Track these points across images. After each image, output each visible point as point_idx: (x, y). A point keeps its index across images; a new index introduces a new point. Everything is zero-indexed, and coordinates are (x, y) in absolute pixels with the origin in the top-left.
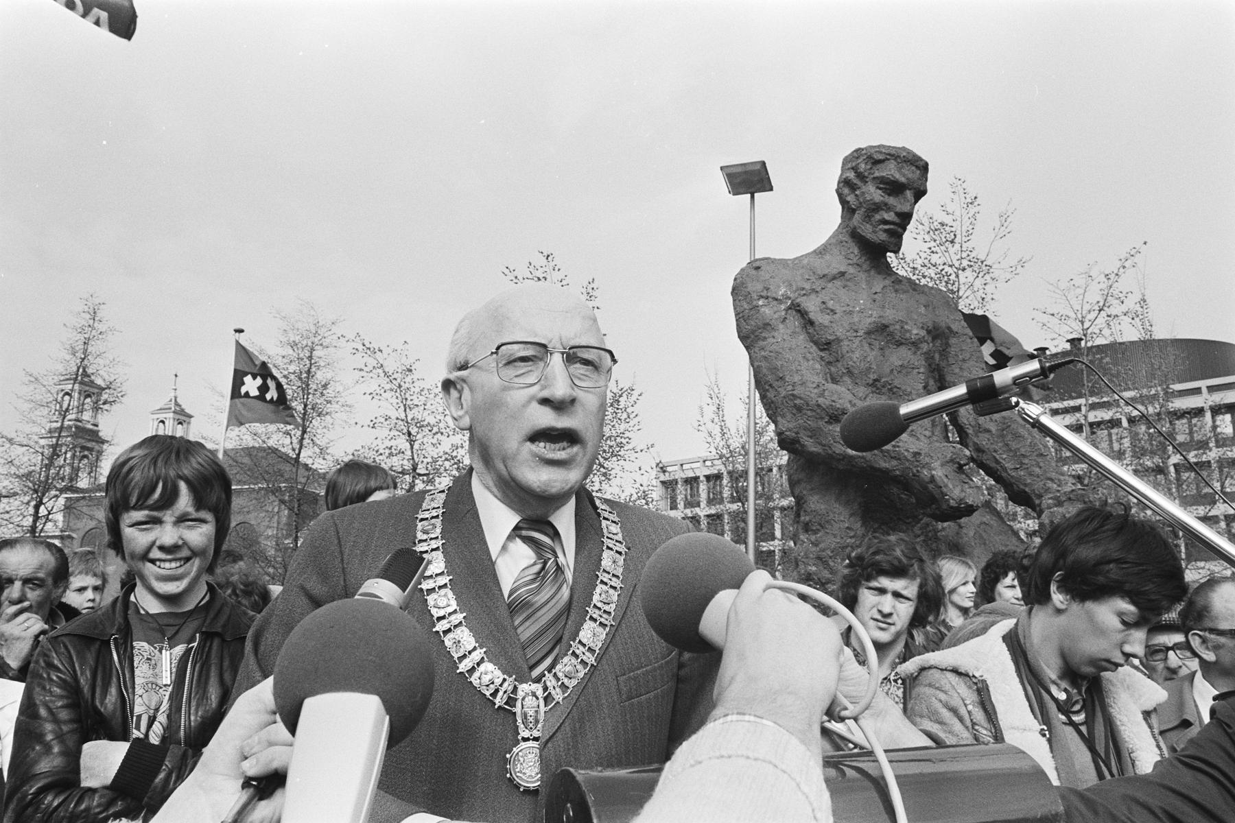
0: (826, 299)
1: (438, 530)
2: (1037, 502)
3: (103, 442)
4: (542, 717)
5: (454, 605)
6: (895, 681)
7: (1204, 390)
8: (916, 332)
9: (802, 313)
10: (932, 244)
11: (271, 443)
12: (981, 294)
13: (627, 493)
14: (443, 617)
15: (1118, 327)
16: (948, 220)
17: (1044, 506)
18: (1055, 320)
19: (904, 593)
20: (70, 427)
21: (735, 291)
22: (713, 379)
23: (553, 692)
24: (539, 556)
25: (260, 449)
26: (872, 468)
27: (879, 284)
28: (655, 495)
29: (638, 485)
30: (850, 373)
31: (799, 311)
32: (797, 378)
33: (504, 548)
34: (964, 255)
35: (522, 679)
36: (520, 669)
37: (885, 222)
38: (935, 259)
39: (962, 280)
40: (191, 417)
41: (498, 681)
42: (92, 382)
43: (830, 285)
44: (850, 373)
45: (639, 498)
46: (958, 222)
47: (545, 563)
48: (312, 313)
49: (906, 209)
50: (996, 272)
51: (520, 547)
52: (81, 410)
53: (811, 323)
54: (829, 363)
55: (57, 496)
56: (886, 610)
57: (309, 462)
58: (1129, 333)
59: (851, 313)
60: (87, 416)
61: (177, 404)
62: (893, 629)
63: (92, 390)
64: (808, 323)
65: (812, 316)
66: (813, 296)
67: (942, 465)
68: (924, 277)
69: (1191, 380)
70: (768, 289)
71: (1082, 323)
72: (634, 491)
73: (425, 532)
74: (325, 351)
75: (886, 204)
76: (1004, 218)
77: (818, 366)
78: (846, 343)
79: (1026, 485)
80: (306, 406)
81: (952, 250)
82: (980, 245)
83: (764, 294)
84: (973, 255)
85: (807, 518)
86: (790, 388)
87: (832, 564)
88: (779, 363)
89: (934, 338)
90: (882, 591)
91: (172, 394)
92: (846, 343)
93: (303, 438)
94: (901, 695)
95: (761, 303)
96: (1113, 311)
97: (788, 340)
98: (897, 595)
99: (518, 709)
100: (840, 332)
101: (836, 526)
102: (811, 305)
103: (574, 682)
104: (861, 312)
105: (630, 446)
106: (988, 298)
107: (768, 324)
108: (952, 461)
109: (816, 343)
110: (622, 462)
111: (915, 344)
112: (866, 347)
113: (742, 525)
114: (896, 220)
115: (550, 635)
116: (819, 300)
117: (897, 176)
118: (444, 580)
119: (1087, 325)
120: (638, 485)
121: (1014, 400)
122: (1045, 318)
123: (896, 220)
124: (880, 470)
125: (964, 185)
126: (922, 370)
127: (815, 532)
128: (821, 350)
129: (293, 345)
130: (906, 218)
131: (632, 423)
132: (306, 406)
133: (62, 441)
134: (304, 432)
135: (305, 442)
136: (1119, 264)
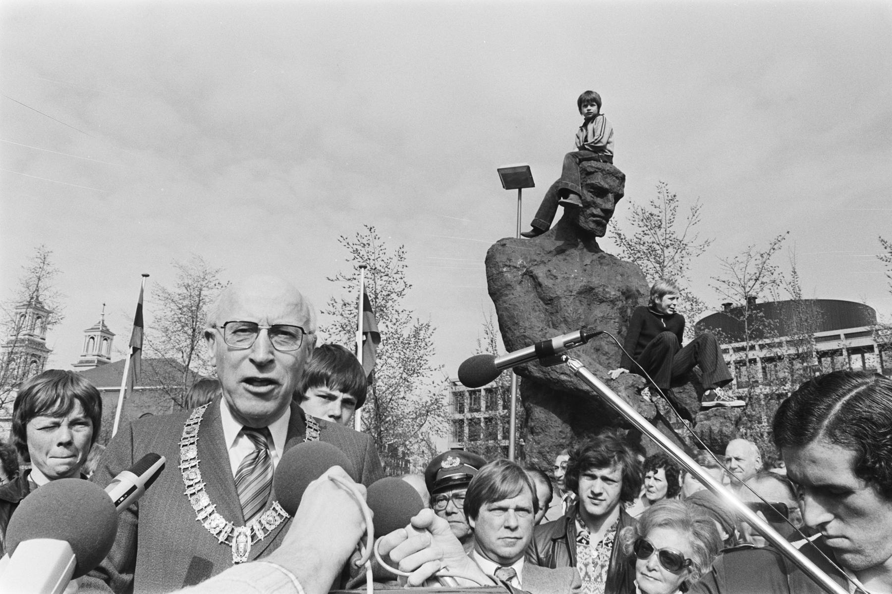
0: (551, 268)
1: (196, 431)
2: (693, 416)
3: (48, 351)
4: (249, 549)
5: (199, 478)
6: (607, 544)
7: (842, 337)
8: (613, 293)
9: (534, 278)
10: (645, 228)
11: (167, 356)
12: (679, 264)
13: (424, 400)
14: (192, 486)
15: (776, 291)
16: (656, 212)
17: (697, 419)
18: (726, 285)
19: (610, 476)
20: (23, 340)
21: (488, 261)
22: (489, 321)
23: (257, 533)
24: (257, 447)
25: (159, 360)
26: (577, 388)
27: (589, 258)
28: (445, 402)
29: (431, 395)
30: (565, 321)
31: (531, 276)
32: (527, 324)
33: (235, 442)
34: (668, 236)
35: (237, 524)
36: (237, 518)
37: (594, 215)
38: (646, 239)
39: (666, 254)
40: (113, 335)
41: (222, 526)
42: (43, 307)
43: (554, 258)
44: (565, 321)
45: (432, 404)
46: (663, 213)
47: (259, 452)
48: (202, 264)
49: (608, 206)
50: (690, 249)
51: (245, 441)
52: (33, 328)
53: (540, 285)
54: (552, 313)
55: (9, 390)
56: (597, 491)
57: (196, 370)
58: (785, 296)
59: (568, 278)
60: (37, 332)
61: (103, 325)
62: (604, 504)
63: (41, 313)
64: (538, 285)
65: (540, 280)
66: (542, 266)
67: (626, 389)
68: (639, 252)
69: (833, 329)
70: (510, 260)
71: (744, 288)
72: (428, 399)
73: (188, 433)
74: (211, 291)
75: (594, 203)
76: (695, 211)
77: (542, 315)
78: (564, 300)
79: (686, 404)
80: (194, 330)
81: (659, 233)
82: (678, 229)
83: (508, 263)
84: (673, 236)
85: (533, 424)
86: (522, 331)
87: (549, 457)
88: (515, 313)
89: (627, 298)
90: (594, 477)
91: (101, 318)
92: (564, 300)
93: (191, 354)
94: (609, 555)
95: (505, 270)
96: (764, 280)
97: (521, 295)
98: (605, 479)
99: (233, 544)
100: (559, 293)
101: (553, 430)
102: (540, 272)
103: (273, 527)
104: (575, 278)
105: (427, 366)
106: (684, 268)
107: (509, 285)
108: (633, 386)
109: (542, 299)
110: (420, 378)
111: (613, 302)
112: (578, 304)
113: (507, 426)
114: (601, 214)
115: (260, 499)
116: (545, 269)
117: (602, 183)
118: (196, 462)
119: (748, 289)
120: (431, 395)
121: (564, 357)
122: (718, 284)
123: (601, 214)
124: (582, 391)
125: (667, 187)
126: (617, 320)
127: (538, 434)
128: (547, 304)
129: (187, 287)
130: (608, 213)
131: (428, 350)
132: (194, 330)
133: (16, 350)
134: (192, 349)
135: (193, 356)
136: (770, 247)
